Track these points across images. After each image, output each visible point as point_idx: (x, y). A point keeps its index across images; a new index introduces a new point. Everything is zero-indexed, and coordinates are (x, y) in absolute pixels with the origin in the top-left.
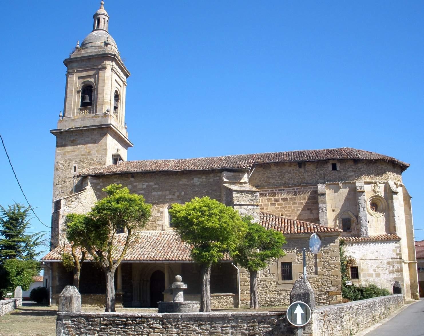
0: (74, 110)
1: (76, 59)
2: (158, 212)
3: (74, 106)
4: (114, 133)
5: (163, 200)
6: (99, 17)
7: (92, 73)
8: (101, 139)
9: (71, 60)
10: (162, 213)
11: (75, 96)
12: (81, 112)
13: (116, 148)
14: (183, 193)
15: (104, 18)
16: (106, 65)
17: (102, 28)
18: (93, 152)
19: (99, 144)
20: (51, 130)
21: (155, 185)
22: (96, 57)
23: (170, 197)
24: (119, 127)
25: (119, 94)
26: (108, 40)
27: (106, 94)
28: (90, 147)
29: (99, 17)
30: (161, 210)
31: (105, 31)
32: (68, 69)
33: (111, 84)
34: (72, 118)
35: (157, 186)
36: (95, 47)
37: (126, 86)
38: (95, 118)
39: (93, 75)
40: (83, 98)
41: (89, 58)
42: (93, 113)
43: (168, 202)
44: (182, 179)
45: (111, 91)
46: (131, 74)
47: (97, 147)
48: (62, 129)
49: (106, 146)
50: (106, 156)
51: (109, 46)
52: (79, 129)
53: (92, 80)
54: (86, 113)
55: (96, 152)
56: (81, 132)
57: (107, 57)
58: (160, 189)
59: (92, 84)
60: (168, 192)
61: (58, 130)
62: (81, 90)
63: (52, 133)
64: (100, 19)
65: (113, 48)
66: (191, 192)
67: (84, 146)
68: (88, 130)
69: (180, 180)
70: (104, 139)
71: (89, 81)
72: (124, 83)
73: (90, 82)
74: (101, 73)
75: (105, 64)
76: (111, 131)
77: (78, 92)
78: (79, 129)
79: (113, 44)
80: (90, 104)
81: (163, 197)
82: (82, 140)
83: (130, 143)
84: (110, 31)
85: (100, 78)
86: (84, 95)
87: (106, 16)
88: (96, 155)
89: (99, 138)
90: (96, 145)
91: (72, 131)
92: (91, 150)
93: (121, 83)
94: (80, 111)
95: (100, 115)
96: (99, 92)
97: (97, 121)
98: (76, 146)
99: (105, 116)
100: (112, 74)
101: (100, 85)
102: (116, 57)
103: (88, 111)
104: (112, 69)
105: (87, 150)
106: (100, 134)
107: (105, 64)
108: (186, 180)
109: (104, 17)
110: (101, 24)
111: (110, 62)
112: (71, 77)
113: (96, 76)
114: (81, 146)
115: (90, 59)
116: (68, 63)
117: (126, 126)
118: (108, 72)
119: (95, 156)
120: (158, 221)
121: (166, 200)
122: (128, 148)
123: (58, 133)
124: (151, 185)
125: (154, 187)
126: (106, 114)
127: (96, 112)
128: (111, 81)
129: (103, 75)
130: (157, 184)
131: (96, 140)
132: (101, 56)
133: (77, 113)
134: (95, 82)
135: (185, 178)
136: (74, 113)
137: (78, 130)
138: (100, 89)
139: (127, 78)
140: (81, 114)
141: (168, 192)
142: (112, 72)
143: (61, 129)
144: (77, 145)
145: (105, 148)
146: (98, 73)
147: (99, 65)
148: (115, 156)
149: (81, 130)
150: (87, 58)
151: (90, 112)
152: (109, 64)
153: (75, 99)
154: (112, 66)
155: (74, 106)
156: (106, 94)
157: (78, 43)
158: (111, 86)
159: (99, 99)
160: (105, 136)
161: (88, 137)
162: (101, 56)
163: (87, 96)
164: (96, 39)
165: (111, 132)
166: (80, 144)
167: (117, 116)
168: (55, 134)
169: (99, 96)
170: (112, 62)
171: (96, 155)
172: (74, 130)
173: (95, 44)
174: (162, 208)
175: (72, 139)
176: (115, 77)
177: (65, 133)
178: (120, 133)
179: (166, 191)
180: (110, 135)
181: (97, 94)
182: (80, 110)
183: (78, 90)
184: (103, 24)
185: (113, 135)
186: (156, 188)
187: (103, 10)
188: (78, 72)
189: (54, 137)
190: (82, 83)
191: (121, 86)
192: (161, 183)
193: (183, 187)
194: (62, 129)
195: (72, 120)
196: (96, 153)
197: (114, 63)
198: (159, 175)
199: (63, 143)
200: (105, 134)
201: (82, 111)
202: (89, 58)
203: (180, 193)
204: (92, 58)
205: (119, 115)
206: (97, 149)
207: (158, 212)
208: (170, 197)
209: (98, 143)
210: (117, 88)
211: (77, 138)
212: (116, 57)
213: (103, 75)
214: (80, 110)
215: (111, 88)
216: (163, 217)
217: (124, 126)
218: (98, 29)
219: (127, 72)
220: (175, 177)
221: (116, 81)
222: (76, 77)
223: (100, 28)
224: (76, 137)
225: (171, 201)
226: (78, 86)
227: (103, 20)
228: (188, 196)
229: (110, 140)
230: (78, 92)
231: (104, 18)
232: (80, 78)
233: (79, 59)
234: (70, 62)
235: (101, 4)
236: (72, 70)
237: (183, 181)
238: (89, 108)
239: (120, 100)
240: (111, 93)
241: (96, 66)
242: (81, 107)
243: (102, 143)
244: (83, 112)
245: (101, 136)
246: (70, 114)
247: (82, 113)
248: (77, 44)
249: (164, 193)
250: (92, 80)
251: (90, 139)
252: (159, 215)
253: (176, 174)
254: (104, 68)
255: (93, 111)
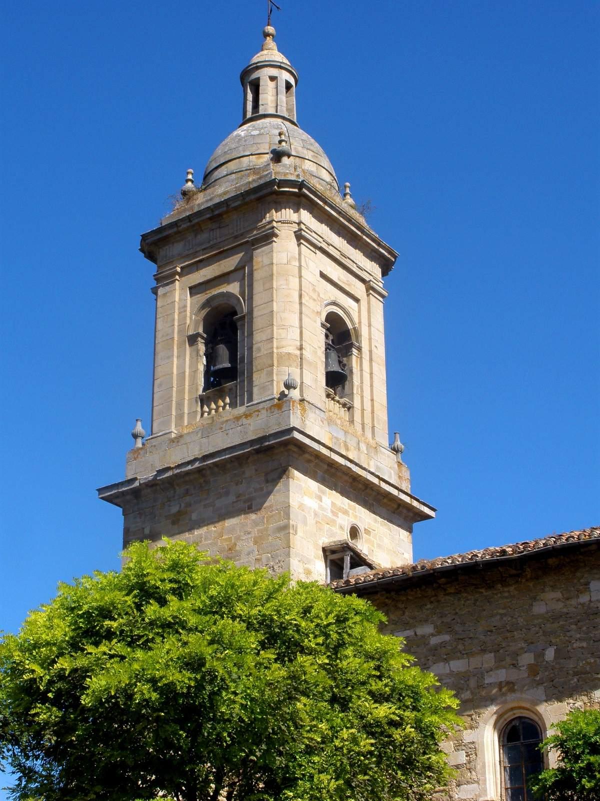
0: (180, 405)
1: (175, 229)
2: (458, 748)
3: (181, 391)
4: (326, 467)
5: (472, 693)
6: (254, 76)
7: (230, 263)
8: (269, 493)
9: (160, 236)
10: (473, 750)
11: (181, 356)
12: (206, 409)
13: (346, 522)
14: (550, 654)
15: (273, 79)
16: (275, 224)
17: (272, 111)
18: (246, 545)
19: (262, 513)
20: (100, 491)
21: (439, 633)
22: (239, 203)
23: (502, 675)
24: (352, 443)
25: (350, 326)
26: (280, 142)
27: (283, 327)
28: (232, 530)
29: (254, 76)
30: (468, 736)
31: (279, 121)
32: (159, 267)
33: (301, 290)
34: (173, 435)
35: (447, 637)
36: (239, 175)
37: (383, 296)
38: (244, 421)
39: (235, 270)
40: (211, 357)
41: (217, 215)
42: (242, 404)
43: (492, 700)
44: (543, 591)
45: (301, 313)
46: (396, 252)
47: (255, 523)
48: (135, 479)
49: (287, 515)
50: (288, 555)
51: (285, 160)
52: (190, 467)
53: (233, 288)
54: (224, 410)
55: (256, 543)
56: (202, 480)
57: (274, 196)
58: (460, 647)
59: (233, 302)
60: (489, 659)
61: (122, 484)
62: (201, 330)
63: (107, 499)
64: (261, 83)
65: (311, 164)
66: (584, 644)
67: (212, 528)
68: (221, 467)
69: (534, 599)
70: (279, 491)
71: (222, 295)
72: (370, 288)
73: (229, 295)
74: (260, 256)
75: (271, 222)
76: (307, 456)
77: (192, 340)
78: (190, 467)
79: (309, 155)
80: (231, 374)
81: (473, 683)
82: (205, 506)
83: (415, 504)
84: (306, 120)
85: (257, 275)
86: (212, 348)
87: (280, 67)
88: (256, 554)
89: (262, 489)
90: (253, 516)
91: (171, 481)
92: (238, 538)
93: (359, 289)
94: (202, 407)
95: (261, 406)
96: (258, 323)
97: (251, 428)
98: (187, 535)
99: (279, 407)
100: (300, 254)
101: (258, 299)
102: (309, 189)
103: (228, 400)
104: (299, 236)
105: (226, 540)
106: (267, 474)
107: (271, 222)
108: (558, 595)
109: (273, 72)
110: (267, 99)
111: (288, 214)
112: (165, 295)
113: (243, 273)
114: (205, 528)
115: (220, 215)
116: (154, 245)
117: (398, 443)
118: (284, 247)
119: (252, 558)
120: (458, 785)
121: (483, 693)
122: (416, 525)
123: (128, 497)
124: (423, 636)
125: (434, 641)
126: (283, 395)
127: (250, 399)
128: (297, 280)
129: (266, 261)
130: (447, 628)
131: (250, 500)
132: (253, 197)
133: (192, 414)
134: (242, 293)
135: (553, 588)
136: (180, 417)
137: (188, 473)
138: (260, 313)
139: (384, 273)
140: (206, 414)
141: (492, 655)
142: (299, 245)
143: (134, 480)
144: (191, 529)
145: (282, 523)
146: (251, 259)
147: (252, 230)
148: (333, 552)
149: (199, 471)
150: (208, 216)
151: (233, 405)
152: (285, 218)
153: (181, 367)
154: (299, 224)
155: (181, 391)
156: (283, 327)
157: (190, 177)
158: (300, 296)
159: (259, 349)
160: (280, 477)
161: (227, 494)
162: (253, 197)
163: (223, 350)
164: (241, 149)
165: (309, 461)
166: (199, 524)
167: (349, 408)
168: (117, 501)
169: (258, 337)
170: (297, 211)
171: (256, 554)
172: (176, 475)
173: (240, 163)
174: (471, 728)
175: (175, 509)
176: (317, 263)
177: (149, 490)
178: (351, 461)
179: (483, 651)
180: (305, 472)
181: (251, 334)
182: (204, 401)
183: (191, 333)
184: (274, 98)
185: (320, 473)
186: (443, 645)
187: (272, 53)
188: (186, 271)
189: (116, 514)
190: (203, 307)
191: (357, 300)
192: (463, 624)
193: (549, 627)
194: (135, 479)
195: (172, 441)
196: (255, 548)
197: (305, 216)
198: (452, 590)
199: (147, 531)
200: (281, 473)
201: (209, 406)
202: (217, 212)
203: (540, 655)
204: (227, 212)
205: (357, 403)
206: (255, 532)
207: (458, 748)
208: (502, 675)
209: (260, 509)
210: (334, 303)
211: (189, 505)
212: (309, 189)
213: (266, 261)
214: (204, 401)
215: (301, 304)
216: (478, 767)
217: (386, 443)
218: (257, 116)
219: (379, 245)
220: (512, 588)
221: (323, 275)
222: (182, 289)
223: (261, 112)
224: (188, 499)
225: (504, 694)
226: (191, 318)
227: (272, 85)
228: (571, 664)
229: (304, 493)
230: (192, 340)
231: (273, 79)
232: (194, 290)
233: (184, 226)
234: (160, 240)
235: (267, 35)
236: (167, 271)
237: (549, 601)
238: (231, 390)
239: (359, 349)
240: (301, 320)
241: (242, 235)
242: (204, 390)
243: (271, 506)
244: (213, 406)
245: (267, 481)
246: (167, 423)
247: (209, 413)
248: (187, 181)
249: (476, 662)
250: (233, 288)
251: (232, 498)
252: (462, 758)
253: (518, 576)
254: (268, 237)
255: (242, 396)
